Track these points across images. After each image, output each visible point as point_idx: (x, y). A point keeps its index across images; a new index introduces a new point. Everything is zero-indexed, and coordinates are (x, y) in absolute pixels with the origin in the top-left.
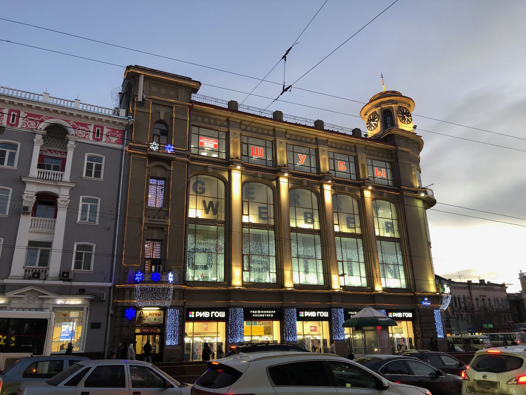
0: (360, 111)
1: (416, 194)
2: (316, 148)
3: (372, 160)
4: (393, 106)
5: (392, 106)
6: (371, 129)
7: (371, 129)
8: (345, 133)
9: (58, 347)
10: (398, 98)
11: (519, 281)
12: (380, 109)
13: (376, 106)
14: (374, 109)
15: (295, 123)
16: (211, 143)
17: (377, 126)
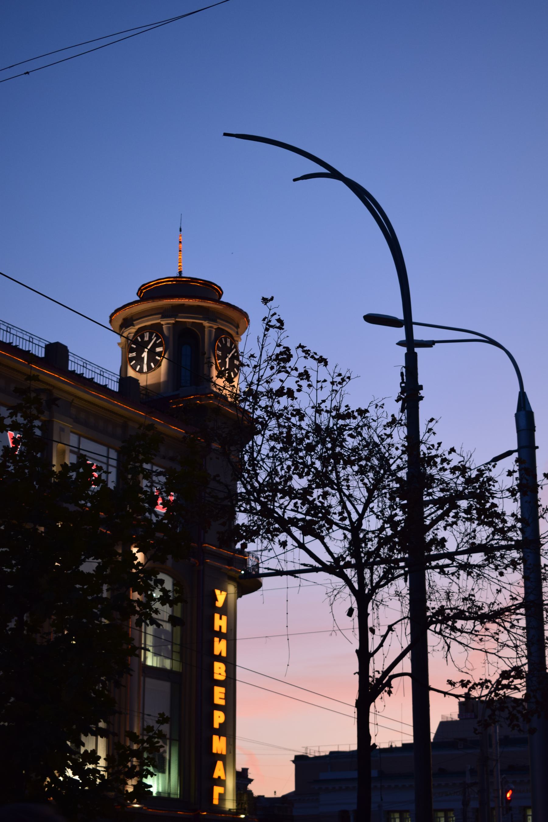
0: (116, 308)
1: (229, 565)
2: (47, 419)
3: (80, 436)
4: (206, 324)
5: (202, 324)
6: (139, 367)
7: (139, 367)
8: (83, 374)
9: (489, 575)
10: (221, 307)
11: (536, 425)
12: (173, 324)
13: (165, 313)
14: (158, 319)
15: (8, 342)
16: (493, 578)
17: (160, 365)
